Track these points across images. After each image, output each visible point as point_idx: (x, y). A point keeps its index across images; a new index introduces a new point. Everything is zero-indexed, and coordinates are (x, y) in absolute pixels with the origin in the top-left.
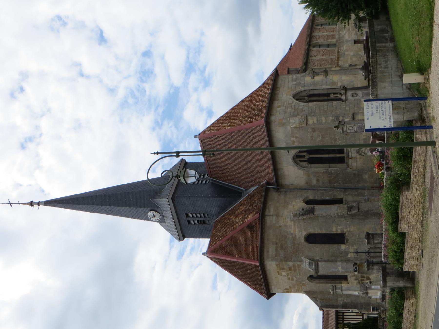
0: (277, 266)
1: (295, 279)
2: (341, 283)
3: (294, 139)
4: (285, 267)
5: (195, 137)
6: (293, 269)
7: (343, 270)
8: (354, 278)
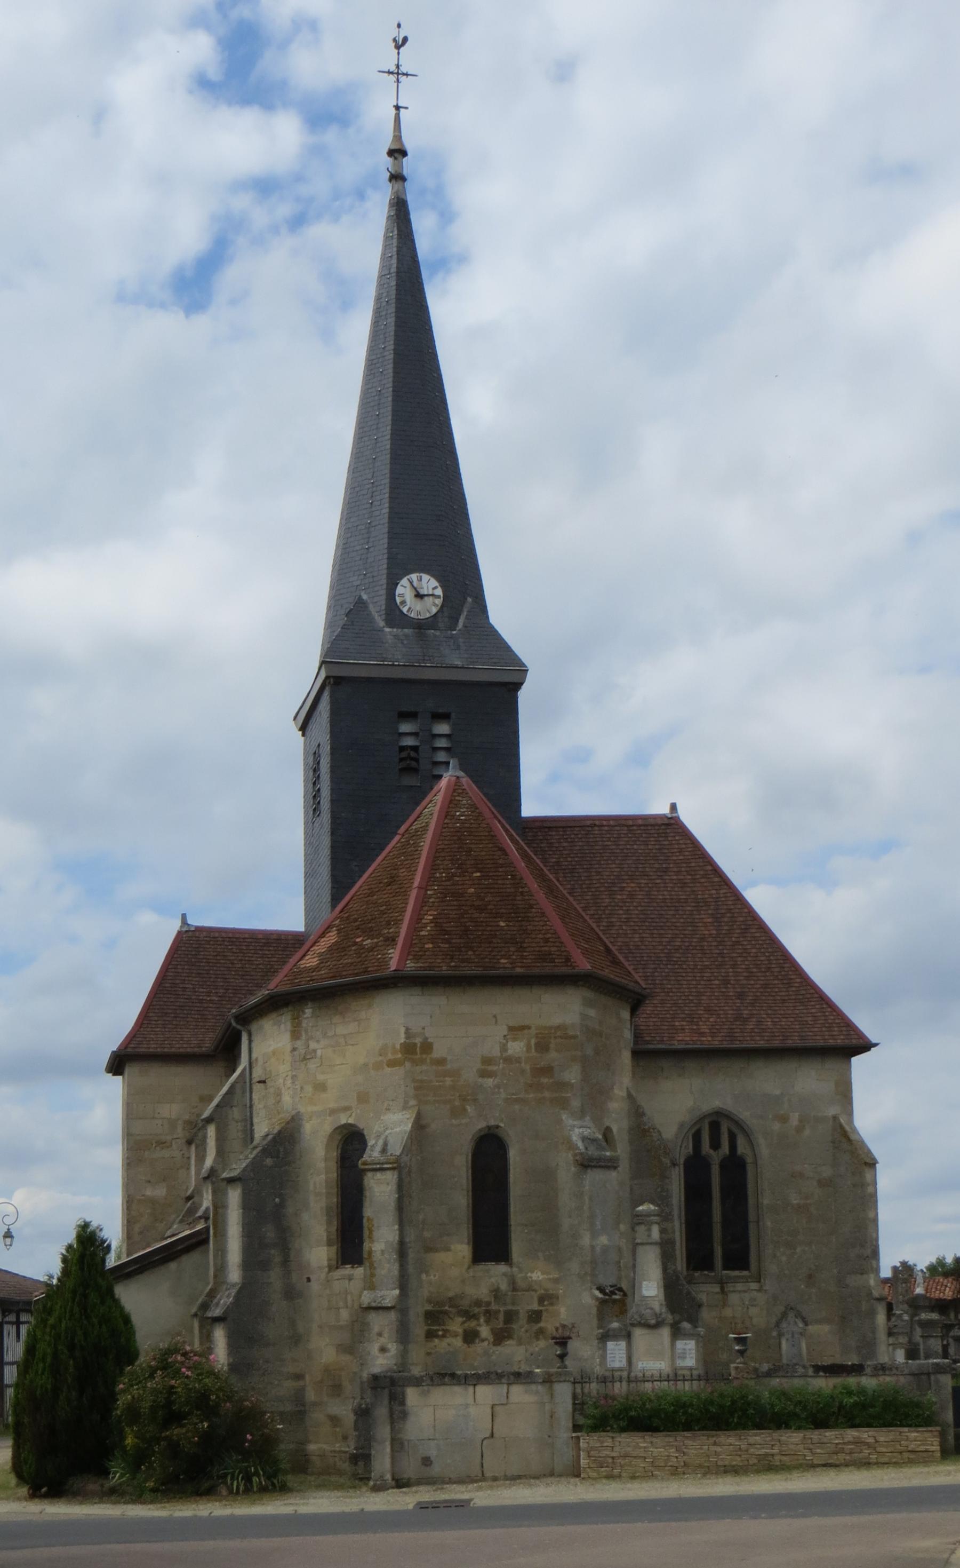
0: (558, 1027)
1: (490, 1082)
2: (329, 1243)
3: (794, 1119)
4: (553, 1055)
5: (673, 807)
6: (545, 1080)
7: (598, 1249)
8: (504, 1287)
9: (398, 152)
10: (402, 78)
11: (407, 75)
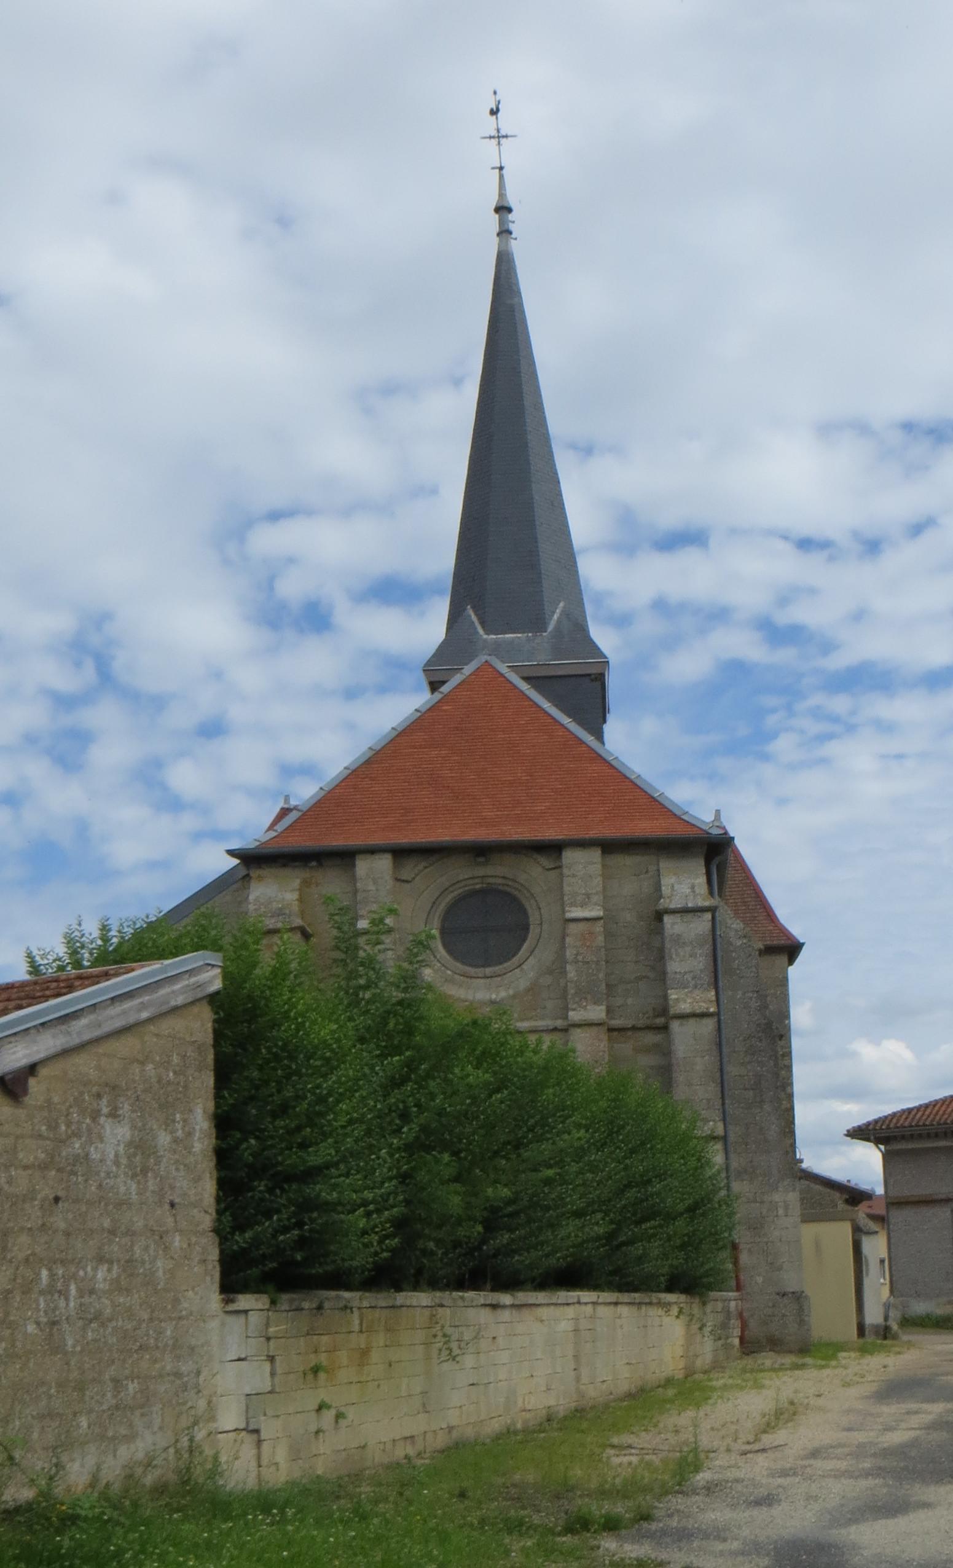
9: (503, 209)
10: (503, 141)
11: (491, 137)
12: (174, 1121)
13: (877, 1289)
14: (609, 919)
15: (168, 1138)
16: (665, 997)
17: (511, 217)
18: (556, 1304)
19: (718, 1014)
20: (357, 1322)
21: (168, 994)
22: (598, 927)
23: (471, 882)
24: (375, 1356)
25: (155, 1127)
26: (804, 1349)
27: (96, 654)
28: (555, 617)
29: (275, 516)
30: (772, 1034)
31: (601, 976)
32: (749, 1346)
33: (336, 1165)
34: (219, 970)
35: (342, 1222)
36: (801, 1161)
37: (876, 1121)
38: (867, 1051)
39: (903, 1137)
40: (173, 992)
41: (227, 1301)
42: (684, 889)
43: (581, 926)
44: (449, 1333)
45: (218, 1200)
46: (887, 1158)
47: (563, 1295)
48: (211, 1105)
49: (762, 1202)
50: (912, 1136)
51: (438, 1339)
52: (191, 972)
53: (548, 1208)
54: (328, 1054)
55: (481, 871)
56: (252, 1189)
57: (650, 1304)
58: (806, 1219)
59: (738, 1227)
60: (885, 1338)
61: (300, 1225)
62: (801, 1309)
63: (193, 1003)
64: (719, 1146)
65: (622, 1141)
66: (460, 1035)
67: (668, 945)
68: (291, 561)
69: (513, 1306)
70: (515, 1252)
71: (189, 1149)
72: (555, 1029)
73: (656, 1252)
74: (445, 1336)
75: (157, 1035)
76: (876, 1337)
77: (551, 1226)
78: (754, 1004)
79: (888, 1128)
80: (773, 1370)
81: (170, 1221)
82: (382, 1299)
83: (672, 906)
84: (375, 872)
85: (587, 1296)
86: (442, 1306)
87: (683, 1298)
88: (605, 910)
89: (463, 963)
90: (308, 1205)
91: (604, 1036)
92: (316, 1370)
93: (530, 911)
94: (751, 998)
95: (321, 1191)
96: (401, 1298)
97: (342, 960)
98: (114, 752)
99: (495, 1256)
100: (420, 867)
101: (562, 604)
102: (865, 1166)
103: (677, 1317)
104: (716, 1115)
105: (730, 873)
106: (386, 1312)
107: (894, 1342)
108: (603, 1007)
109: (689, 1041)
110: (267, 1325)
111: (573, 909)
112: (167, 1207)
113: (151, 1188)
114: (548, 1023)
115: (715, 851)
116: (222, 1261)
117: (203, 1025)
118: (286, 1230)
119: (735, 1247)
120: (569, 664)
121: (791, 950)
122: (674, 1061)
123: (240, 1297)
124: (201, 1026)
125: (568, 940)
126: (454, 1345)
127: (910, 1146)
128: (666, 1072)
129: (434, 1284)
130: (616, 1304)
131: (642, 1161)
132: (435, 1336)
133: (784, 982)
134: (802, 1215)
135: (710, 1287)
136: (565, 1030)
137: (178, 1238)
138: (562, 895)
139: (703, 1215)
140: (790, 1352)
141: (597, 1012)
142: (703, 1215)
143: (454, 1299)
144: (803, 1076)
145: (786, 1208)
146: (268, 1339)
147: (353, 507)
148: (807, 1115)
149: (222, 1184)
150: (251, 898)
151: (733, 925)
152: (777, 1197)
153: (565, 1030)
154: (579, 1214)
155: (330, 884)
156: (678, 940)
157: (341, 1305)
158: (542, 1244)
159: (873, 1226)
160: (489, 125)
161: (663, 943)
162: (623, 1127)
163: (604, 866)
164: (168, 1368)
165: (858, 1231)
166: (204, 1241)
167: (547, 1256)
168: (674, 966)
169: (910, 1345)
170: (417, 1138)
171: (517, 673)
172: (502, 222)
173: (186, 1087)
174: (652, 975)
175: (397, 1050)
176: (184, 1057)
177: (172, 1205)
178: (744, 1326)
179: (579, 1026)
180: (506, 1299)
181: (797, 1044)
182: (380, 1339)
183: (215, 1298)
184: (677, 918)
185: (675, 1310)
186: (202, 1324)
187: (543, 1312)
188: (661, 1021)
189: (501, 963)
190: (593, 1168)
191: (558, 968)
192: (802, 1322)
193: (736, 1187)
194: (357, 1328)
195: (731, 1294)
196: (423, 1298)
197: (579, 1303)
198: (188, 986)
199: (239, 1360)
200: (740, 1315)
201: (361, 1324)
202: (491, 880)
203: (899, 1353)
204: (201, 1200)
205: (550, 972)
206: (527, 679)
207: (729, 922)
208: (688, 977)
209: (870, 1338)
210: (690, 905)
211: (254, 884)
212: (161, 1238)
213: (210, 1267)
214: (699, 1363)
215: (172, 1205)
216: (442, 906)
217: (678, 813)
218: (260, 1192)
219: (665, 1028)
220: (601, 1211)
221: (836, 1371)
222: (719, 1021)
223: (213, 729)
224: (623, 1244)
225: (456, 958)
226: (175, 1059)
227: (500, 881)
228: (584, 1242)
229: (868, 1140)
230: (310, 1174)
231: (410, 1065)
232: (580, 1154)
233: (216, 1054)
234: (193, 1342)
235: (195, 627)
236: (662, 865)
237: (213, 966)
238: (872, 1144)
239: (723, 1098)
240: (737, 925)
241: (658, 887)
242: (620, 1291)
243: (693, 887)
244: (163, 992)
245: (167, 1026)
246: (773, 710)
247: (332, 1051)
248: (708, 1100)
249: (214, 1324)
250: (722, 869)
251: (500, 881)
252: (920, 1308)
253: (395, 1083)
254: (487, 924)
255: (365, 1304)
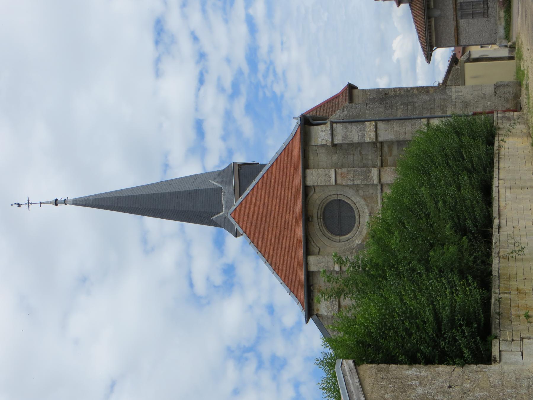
9: (56, 203)
11: (29, 207)
12: (411, 385)
13: (491, 51)
14: (336, 167)
15: (419, 388)
16: (369, 143)
17: (59, 199)
18: (499, 198)
19: (376, 121)
20: (506, 295)
21: (354, 387)
22: (339, 171)
23: (320, 224)
24: (521, 287)
25: (414, 395)
26: (519, 84)
27: (242, 353)
28: (215, 184)
29: (191, 285)
30: (384, 97)
31: (359, 170)
32: (518, 108)
33: (434, 306)
34: (344, 361)
35: (460, 305)
36: (439, 84)
37: (424, 51)
38: (397, 55)
39: (430, 39)
40: (353, 384)
41: (495, 361)
42: (323, 135)
43: (338, 178)
44: (511, 251)
45: (448, 364)
46: (439, 46)
47: (495, 194)
48: (405, 366)
49: (456, 102)
50: (430, 36)
51: (514, 256)
52: (344, 375)
53: (456, 202)
54: (384, 308)
55: (316, 219)
56: (444, 348)
57: (499, 153)
58: (464, 83)
59: (466, 113)
60: (515, 48)
61: (461, 326)
62: (502, 86)
63: (358, 374)
64: (432, 121)
65: (428, 166)
66: (378, 244)
67: (347, 142)
68: (208, 279)
69: (499, 218)
70: (475, 217)
71: (425, 378)
72: (382, 189)
73: (476, 151)
74: (512, 252)
75: (372, 392)
76: (514, 53)
77: (464, 200)
78: (372, 105)
79: (426, 46)
80: (528, 98)
81: (457, 388)
82: (495, 283)
83: (330, 140)
84: (316, 263)
85: (495, 183)
86: (499, 253)
87: (496, 138)
88: (332, 168)
89: (353, 227)
90: (452, 320)
91: (385, 169)
92: (527, 316)
93: (332, 199)
94: (369, 107)
95: (445, 314)
96: (495, 273)
97: (345, 295)
98: (278, 346)
99: (477, 226)
100: (313, 244)
101: (211, 181)
102: (442, 55)
103: (505, 142)
104: (418, 121)
105: (318, 114)
106: (501, 280)
107: (517, 44)
108: (373, 169)
109: (387, 133)
110: (507, 341)
111: (331, 181)
112: (451, 390)
113: (442, 397)
114: (379, 191)
115: (308, 121)
116: (476, 364)
117: (369, 369)
118: (463, 332)
119: (475, 114)
120: (235, 178)
121: (351, 88)
122: (395, 139)
123: (493, 354)
124: (369, 370)
125: (344, 184)
126: (517, 249)
127: (434, 37)
128: (400, 143)
129: (489, 255)
130: (499, 169)
131: (437, 158)
132: (512, 257)
133: (364, 91)
134: (462, 85)
135: (492, 125)
136: (382, 185)
137: (465, 385)
138: (325, 186)
139: (461, 129)
140: (520, 90)
141: (374, 172)
142: (461, 129)
143: (496, 247)
144: (407, 83)
145: (458, 92)
146: (513, 340)
147: (188, 255)
148: (422, 80)
149: (441, 362)
150: (325, 314)
151: (339, 114)
152: (454, 96)
153: (382, 185)
154: (459, 188)
155: (321, 282)
156: (344, 138)
157: (498, 303)
158: (472, 205)
159: (467, 53)
160: (24, 207)
161: (346, 144)
162: (422, 166)
163: (314, 168)
164: (525, 391)
165: (470, 60)
166: (467, 372)
167: (477, 202)
168: (355, 139)
169: (517, 38)
170: (424, 265)
171: (238, 199)
172: (61, 203)
173: (396, 378)
174: (359, 148)
175: (384, 271)
176: (383, 379)
177: (450, 387)
178: (509, 110)
179: (380, 179)
180: (496, 222)
181: (394, 85)
182: (513, 284)
183: (494, 367)
184: (335, 138)
185: (502, 143)
186: (506, 374)
187: (502, 204)
188: (378, 145)
189: (354, 211)
190: (439, 180)
191: (356, 188)
192: (508, 85)
193: (449, 113)
194: (508, 295)
195: (495, 116)
196: (495, 262)
197: (498, 187)
198: (350, 376)
199: (522, 355)
200: (504, 112)
201: (506, 293)
202: (319, 215)
203: (522, 43)
204: (448, 372)
205: (357, 191)
206: (240, 195)
207: (337, 116)
208: (360, 133)
209: (515, 54)
210: (330, 132)
211: (320, 313)
212: (465, 393)
213: (479, 369)
214: (525, 131)
215: (450, 387)
216: (330, 235)
217: (292, 137)
218: (445, 344)
219: (381, 143)
220: (458, 177)
221: (530, 71)
222: (379, 120)
223: (271, 309)
224: (473, 165)
225: (351, 230)
226: (384, 383)
227: (319, 211)
228: (471, 184)
229: (431, 54)
230: (438, 321)
231: (391, 267)
232: (433, 186)
233: (382, 363)
234: (514, 378)
235: (232, 316)
236: (313, 144)
237: (342, 364)
238: (433, 53)
239: (411, 119)
240: (338, 112)
241: (323, 146)
242: (493, 167)
243: (322, 131)
244: (352, 388)
245: (368, 387)
246: (264, 93)
247: (383, 305)
248: (412, 125)
249: (506, 368)
250: (315, 119)
251: (319, 211)
252: (501, 32)
253: (399, 274)
254: (337, 217)
255: (497, 291)
